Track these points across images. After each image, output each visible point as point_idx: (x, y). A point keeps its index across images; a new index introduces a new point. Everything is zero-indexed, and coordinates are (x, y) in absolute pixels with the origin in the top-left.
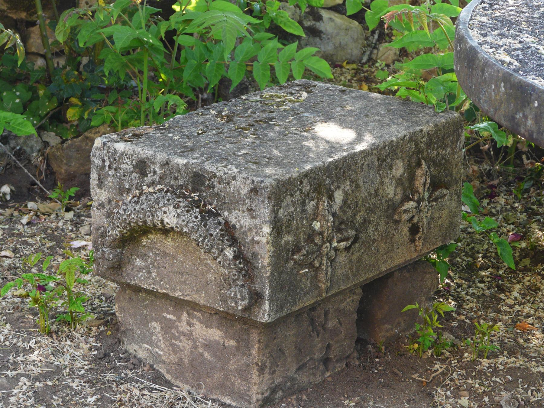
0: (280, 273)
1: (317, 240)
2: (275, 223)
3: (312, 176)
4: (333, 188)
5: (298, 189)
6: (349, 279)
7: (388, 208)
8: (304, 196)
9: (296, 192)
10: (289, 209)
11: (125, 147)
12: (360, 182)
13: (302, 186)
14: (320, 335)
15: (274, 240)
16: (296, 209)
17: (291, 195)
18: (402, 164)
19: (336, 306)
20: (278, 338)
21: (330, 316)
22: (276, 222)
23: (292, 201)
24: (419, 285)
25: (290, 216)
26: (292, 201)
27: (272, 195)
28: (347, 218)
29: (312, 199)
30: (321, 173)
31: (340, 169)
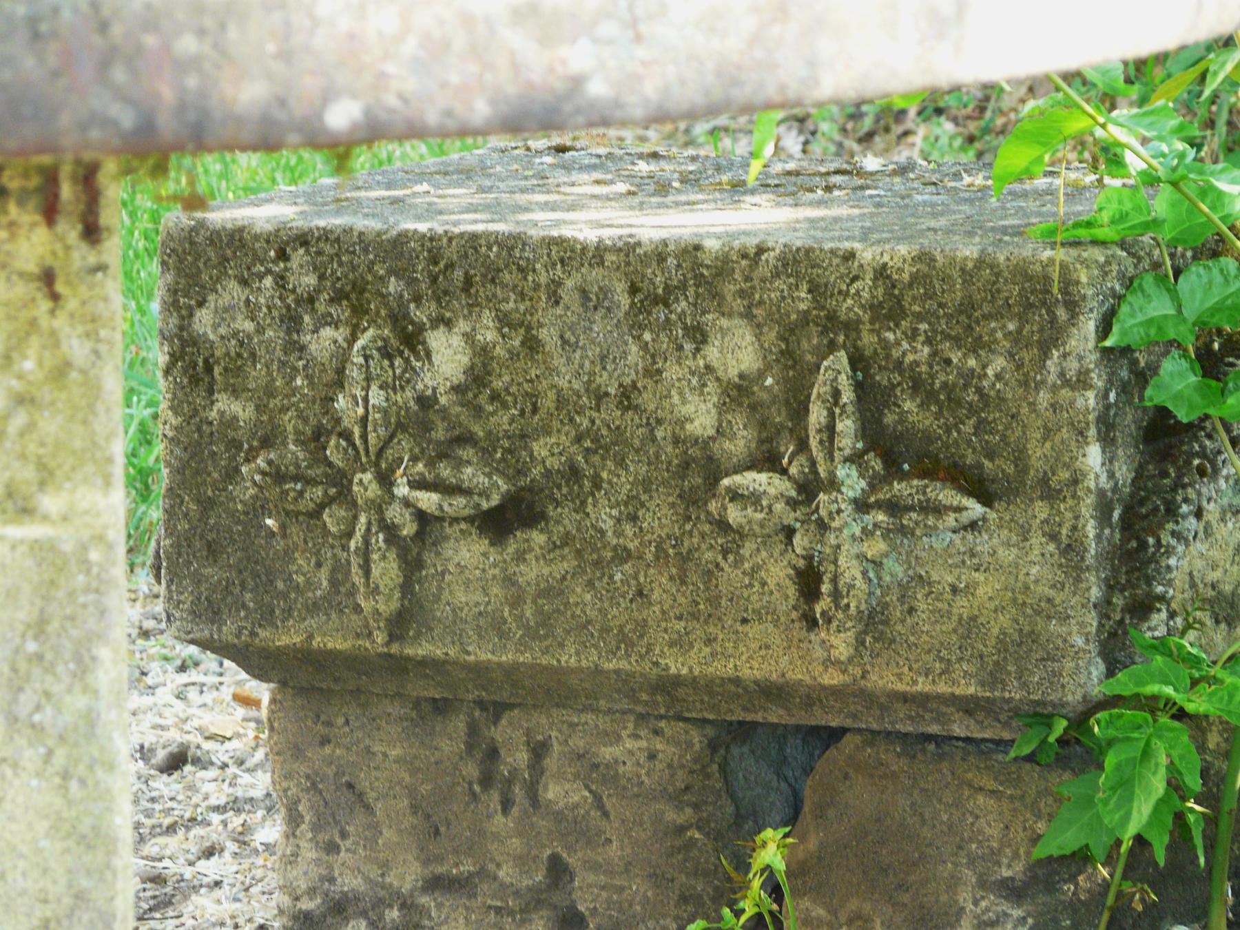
0: (207, 505)
1: (334, 452)
2: (183, 347)
3: (328, 249)
4: (419, 314)
5: (269, 271)
6: (502, 635)
7: (686, 465)
8: (298, 302)
9: (261, 277)
10: (234, 319)
11: (1152, 197)
12: (548, 335)
13: (286, 269)
14: (515, 810)
15: (180, 394)
16: (260, 330)
17: (244, 283)
18: (749, 338)
19: (578, 743)
20: (338, 745)
21: (551, 762)
22: (184, 343)
23: (248, 301)
24: (945, 817)
25: (241, 344)
26: (248, 301)
27: (169, 256)
28: (489, 433)
29: (327, 320)
30: (366, 251)
31: (450, 266)
